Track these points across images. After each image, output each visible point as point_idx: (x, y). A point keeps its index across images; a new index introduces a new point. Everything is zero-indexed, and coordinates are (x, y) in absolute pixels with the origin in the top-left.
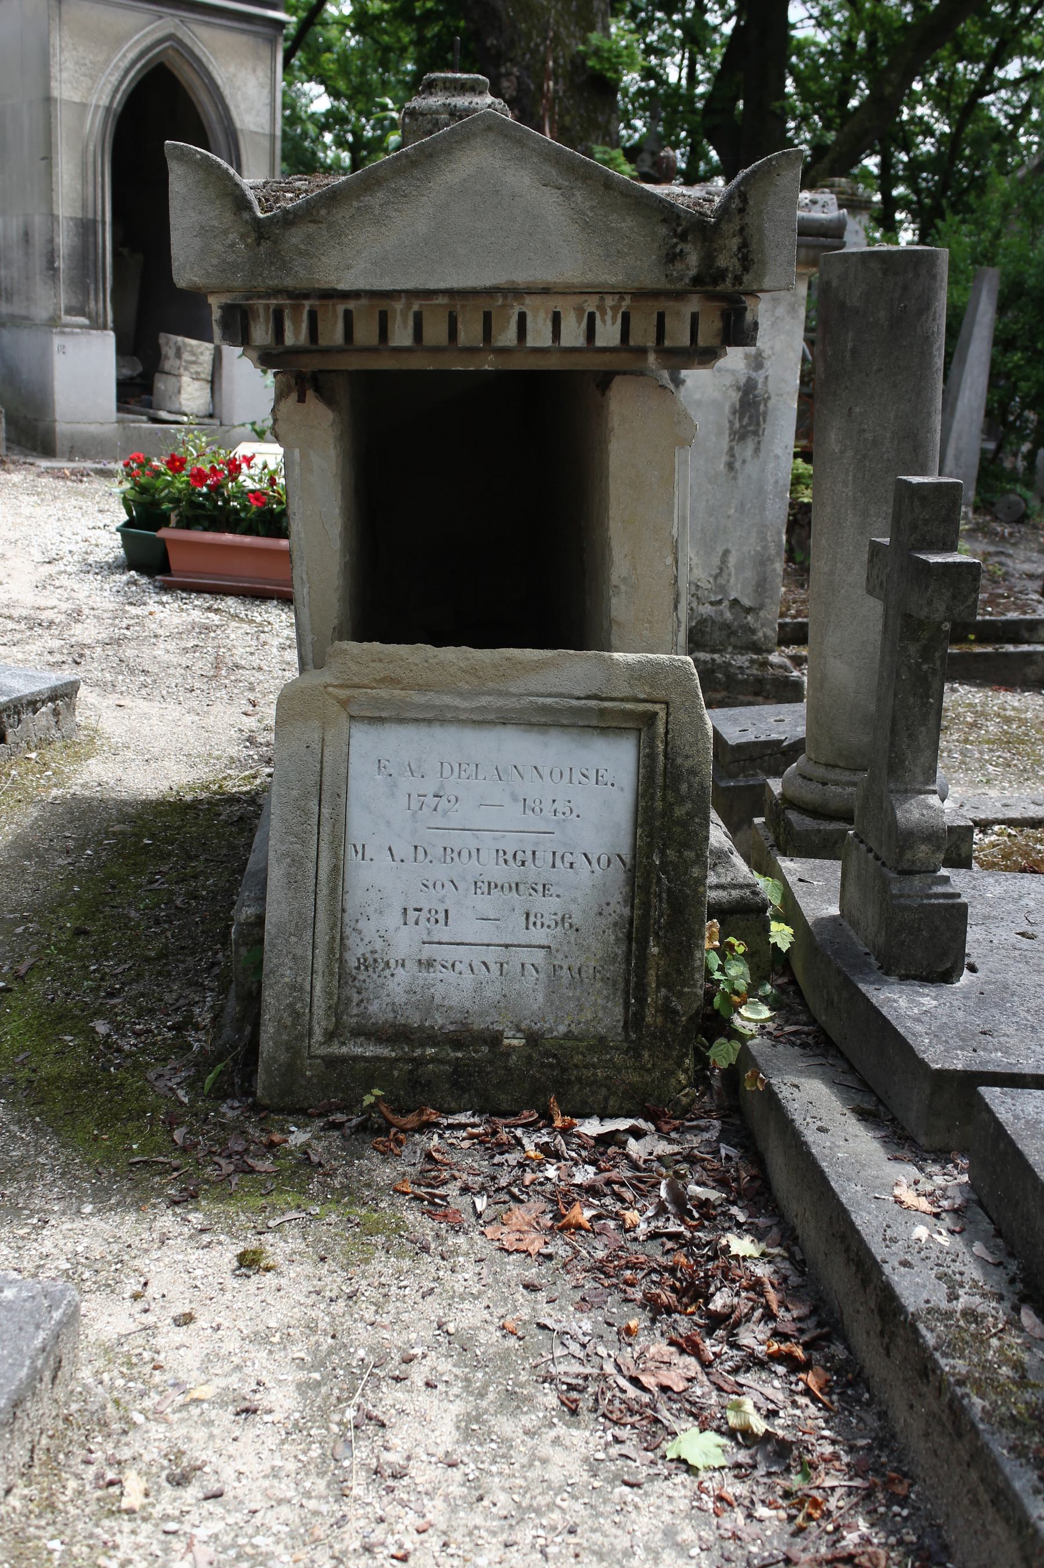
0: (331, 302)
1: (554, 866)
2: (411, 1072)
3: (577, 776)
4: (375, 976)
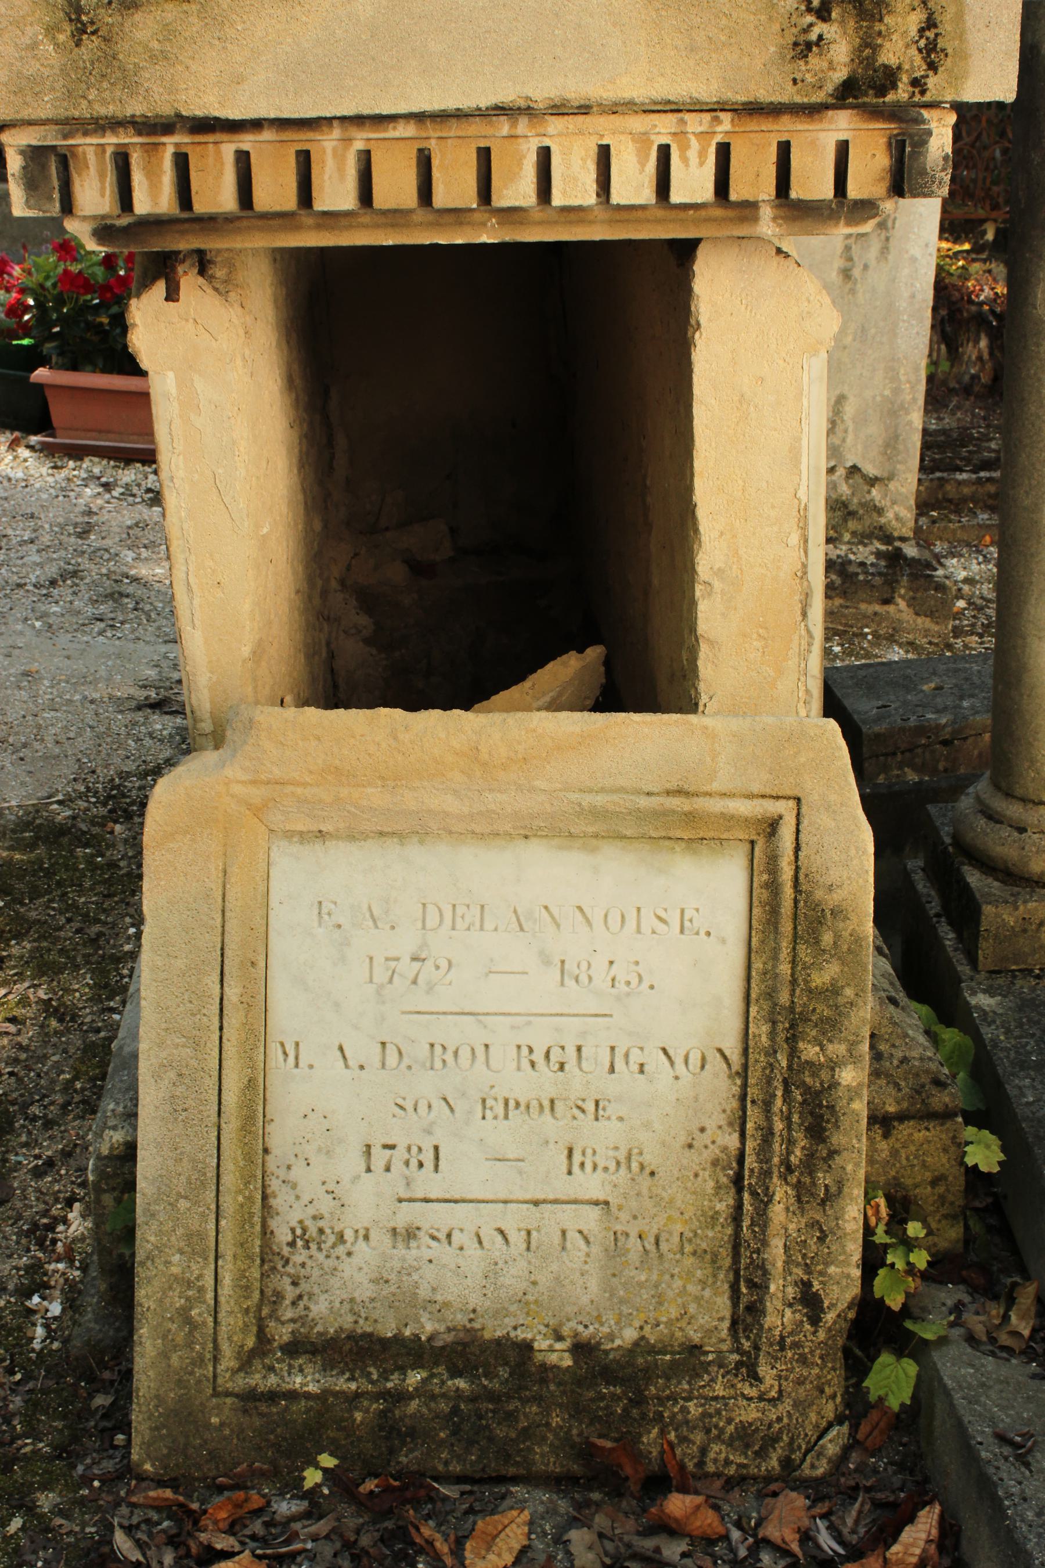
0: (210, 138)
1: (612, 1070)
2: (383, 1414)
3: (649, 921)
4: (320, 1257)
